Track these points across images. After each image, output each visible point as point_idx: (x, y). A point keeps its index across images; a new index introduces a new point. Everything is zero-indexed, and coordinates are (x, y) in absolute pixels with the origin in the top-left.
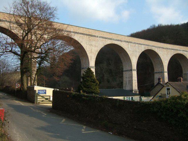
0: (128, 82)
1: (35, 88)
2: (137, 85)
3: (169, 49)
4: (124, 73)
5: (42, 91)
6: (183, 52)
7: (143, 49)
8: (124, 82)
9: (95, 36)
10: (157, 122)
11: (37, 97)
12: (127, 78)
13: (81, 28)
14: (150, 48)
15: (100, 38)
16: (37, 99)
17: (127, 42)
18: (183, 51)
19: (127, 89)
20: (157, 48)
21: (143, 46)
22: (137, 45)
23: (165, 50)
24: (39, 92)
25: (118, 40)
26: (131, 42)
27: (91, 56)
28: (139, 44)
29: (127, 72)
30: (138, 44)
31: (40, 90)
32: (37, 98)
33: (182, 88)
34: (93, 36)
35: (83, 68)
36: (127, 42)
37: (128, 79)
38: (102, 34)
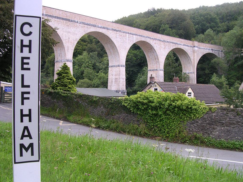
0: (114, 81)
1: (1, 85)
2: (125, 84)
3: (168, 42)
4: (110, 69)
5: (10, 88)
6: (183, 46)
7: (135, 40)
8: (109, 81)
9: (74, 21)
10: (127, 115)
11: (4, 95)
12: (112, 75)
13: (57, 11)
14: (143, 39)
15: (80, 24)
16: (4, 97)
17: (115, 30)
18: (184, 45)
19: (112, 89)
20: (152, 40)
21: (135, 36)
22: (127, 34)
23: (162, 43)
24: (6, 90)
25: (104, 28)
26: (120, 31)
27: (68, 47)
28: (130, 34)
29: (114, 68)
30: (128, 33)
31: (7, 87)
32: (4, 96)
33: (186, 90)
34: (72, 21)
35: (57, 62)
36: (115, 30)
37: (114, 77)
38: (111, 167)
